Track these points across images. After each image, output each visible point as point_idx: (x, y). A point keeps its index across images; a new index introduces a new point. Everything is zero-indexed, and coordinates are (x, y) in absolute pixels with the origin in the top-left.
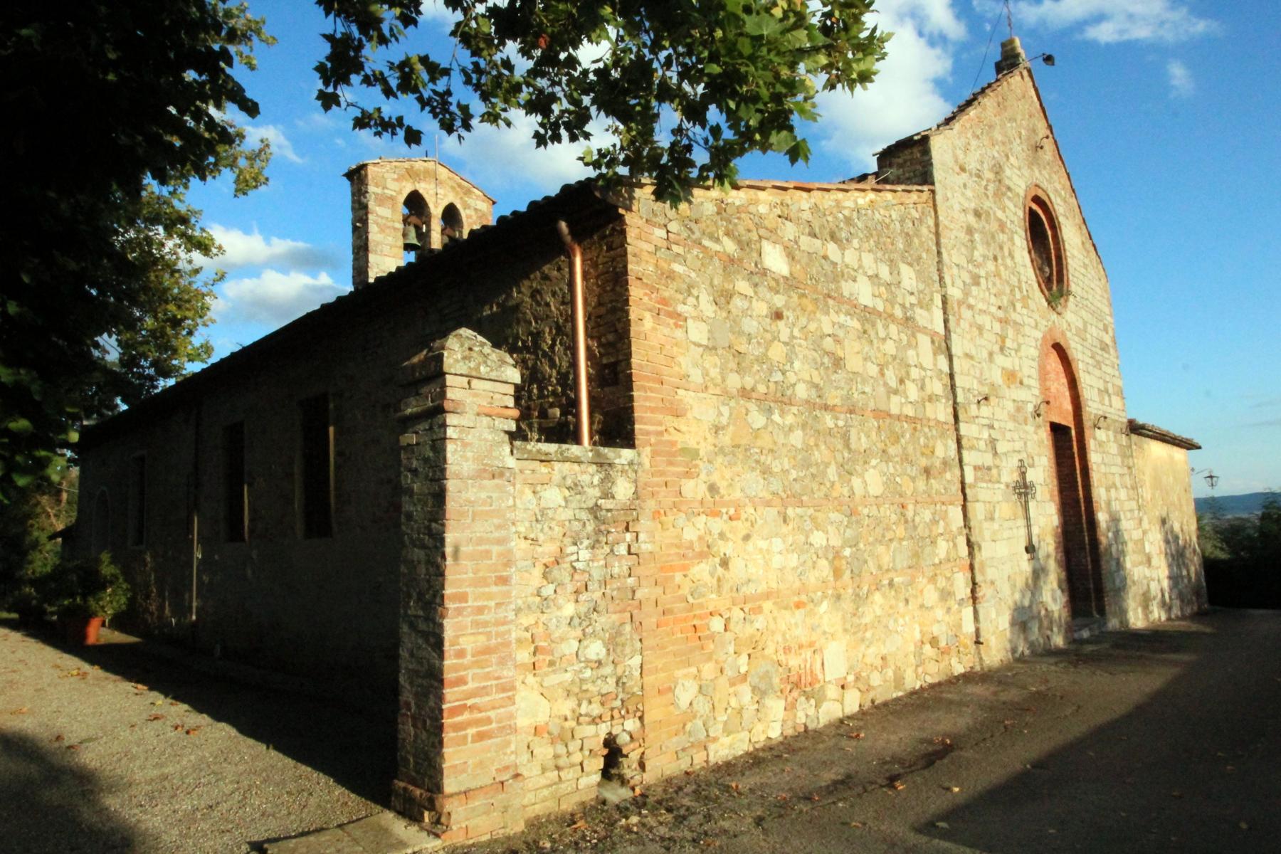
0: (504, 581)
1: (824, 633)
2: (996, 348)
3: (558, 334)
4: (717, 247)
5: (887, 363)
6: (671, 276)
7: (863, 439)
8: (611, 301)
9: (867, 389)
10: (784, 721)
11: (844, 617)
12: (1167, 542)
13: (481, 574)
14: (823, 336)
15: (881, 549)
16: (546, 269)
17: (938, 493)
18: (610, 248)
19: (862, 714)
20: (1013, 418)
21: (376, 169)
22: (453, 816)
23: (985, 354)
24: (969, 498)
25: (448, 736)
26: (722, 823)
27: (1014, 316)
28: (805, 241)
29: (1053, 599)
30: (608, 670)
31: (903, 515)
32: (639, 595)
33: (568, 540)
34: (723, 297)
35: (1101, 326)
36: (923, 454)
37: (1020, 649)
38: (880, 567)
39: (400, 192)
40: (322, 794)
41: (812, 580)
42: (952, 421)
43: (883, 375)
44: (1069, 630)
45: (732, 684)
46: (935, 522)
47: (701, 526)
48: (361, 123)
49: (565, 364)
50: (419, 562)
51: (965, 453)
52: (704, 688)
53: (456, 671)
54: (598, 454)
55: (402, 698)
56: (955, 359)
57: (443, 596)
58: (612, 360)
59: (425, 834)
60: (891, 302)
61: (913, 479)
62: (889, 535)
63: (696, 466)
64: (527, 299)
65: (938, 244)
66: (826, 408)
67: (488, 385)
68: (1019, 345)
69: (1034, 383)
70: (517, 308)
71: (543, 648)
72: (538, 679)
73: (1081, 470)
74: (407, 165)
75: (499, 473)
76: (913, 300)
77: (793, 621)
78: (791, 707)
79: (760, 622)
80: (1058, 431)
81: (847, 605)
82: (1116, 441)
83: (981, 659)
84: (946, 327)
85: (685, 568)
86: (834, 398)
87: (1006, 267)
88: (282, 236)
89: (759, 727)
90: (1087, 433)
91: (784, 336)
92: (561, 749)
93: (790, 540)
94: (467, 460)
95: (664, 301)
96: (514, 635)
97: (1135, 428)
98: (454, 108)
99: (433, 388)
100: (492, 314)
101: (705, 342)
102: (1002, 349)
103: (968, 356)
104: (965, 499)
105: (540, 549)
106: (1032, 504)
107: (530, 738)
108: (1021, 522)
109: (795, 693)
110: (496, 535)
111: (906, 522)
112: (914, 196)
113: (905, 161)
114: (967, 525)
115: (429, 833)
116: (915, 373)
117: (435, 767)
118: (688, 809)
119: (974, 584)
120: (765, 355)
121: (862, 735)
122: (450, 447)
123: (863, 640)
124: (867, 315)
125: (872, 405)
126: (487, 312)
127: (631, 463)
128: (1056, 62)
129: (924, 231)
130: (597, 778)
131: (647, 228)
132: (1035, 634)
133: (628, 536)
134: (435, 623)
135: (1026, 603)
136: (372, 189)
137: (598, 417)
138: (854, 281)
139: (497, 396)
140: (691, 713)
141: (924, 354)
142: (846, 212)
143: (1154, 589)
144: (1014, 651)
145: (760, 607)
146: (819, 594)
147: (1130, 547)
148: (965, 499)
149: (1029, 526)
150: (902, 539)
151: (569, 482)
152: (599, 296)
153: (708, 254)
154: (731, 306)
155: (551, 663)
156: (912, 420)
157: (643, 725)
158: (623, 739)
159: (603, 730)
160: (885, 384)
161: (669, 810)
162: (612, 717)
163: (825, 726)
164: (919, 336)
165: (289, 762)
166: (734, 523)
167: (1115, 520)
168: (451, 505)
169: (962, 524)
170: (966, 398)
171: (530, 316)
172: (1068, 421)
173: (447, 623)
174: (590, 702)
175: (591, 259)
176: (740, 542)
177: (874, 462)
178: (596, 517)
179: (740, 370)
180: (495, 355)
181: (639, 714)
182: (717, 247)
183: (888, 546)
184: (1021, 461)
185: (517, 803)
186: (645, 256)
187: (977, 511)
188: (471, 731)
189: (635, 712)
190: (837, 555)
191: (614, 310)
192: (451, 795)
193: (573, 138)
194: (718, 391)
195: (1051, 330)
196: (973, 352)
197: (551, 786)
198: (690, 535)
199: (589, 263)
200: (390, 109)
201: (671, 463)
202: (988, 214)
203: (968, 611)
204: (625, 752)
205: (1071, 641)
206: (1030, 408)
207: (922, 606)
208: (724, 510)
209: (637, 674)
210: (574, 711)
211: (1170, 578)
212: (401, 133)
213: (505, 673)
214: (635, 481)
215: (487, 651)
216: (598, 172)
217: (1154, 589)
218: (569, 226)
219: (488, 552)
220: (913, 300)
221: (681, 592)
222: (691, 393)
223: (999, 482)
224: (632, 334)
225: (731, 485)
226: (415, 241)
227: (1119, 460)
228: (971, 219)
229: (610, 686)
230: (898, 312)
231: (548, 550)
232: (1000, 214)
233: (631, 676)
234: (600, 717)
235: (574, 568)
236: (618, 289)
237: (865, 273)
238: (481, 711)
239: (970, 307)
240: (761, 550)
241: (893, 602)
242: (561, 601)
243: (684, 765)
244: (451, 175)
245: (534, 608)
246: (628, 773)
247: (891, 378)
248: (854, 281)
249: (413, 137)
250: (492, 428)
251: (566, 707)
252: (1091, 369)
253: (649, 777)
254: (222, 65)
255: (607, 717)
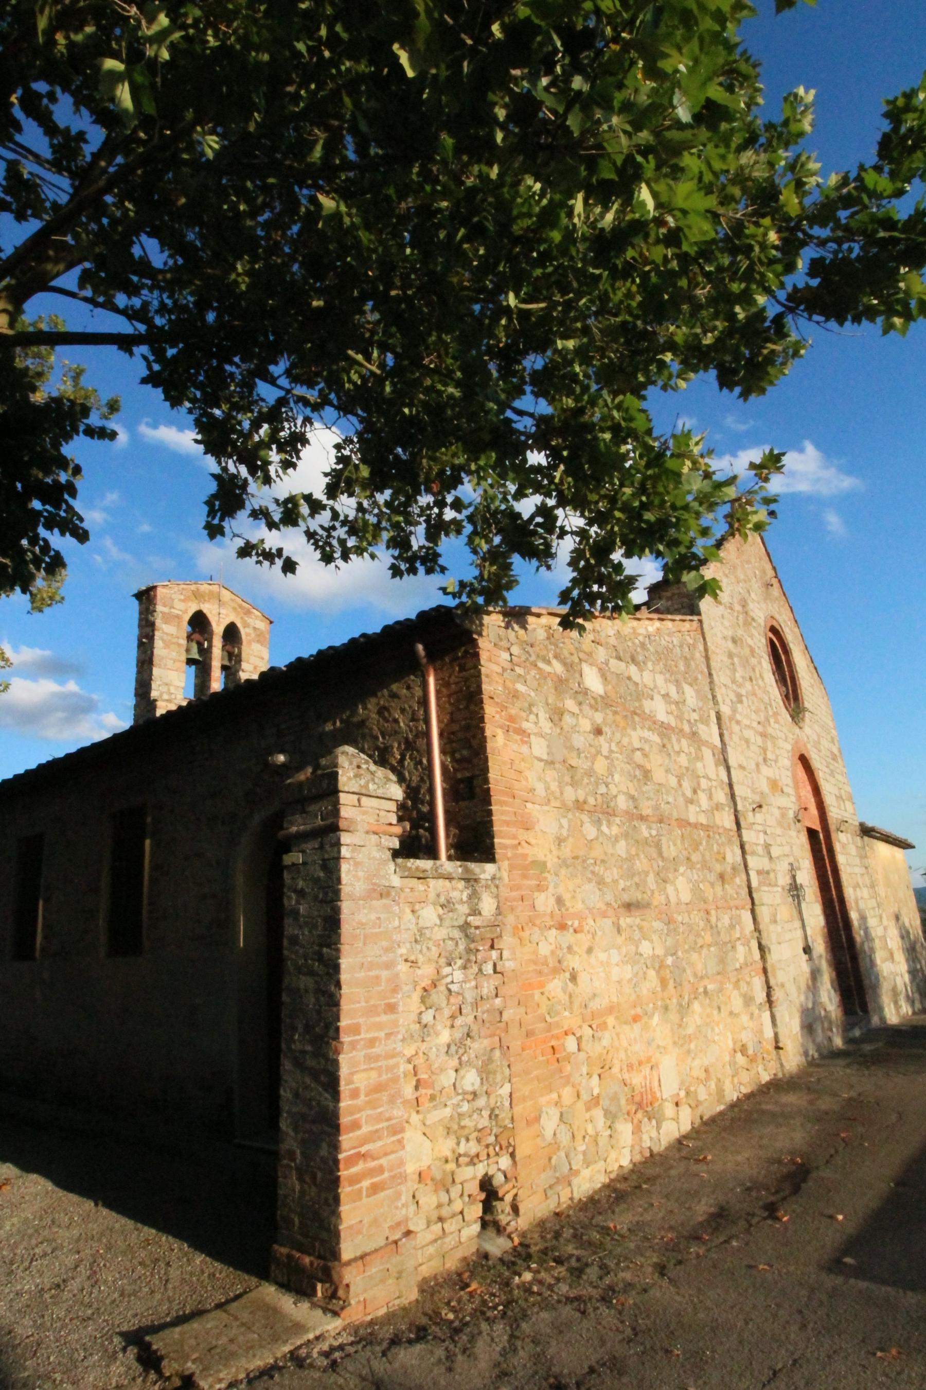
0: (391, 1008)
1: (658, 1047)
2: (761, 759)
3: (407, 749)
4: (547, 669)
5: (683, 774)
6: (516, 695)
7: (672, 847)
8: (465, 719)
9: (671, 800)
10: (632, 1146)
11: (672, 1030)
12: (902, 937)
13: (372, 1002)
14: (634, 750)
15: (694, 956)
16: (394, 687)
17: (732, 898)
18: (462, 668)
19: (695, 1133)
20: (780, 824)
21: (164, 590)
22: (352, 1288)
23: (753, 766)
24: (756, 902)
25: (345, 1191)
26: (621, 1275)
27: (770, 731)
28: (613, 662)
29: (829, 999)
30: (481, 1102)
31: (708, 921)
32: (506, 1016)
33: (442, 961)
34: (557, 715)
35: (829, 738)
36: (717, 860)
37: (811, 1053)
38: (695, 975)
39: (185, 612)
40: (179, 1269)
41: (645, 992)
42: (735, 828)
43: (680, 786)
44: (847, 1027)
45: (588, 1109)
46: (732, 927)
47: (552, 940)
48: (244, 552)
49: (415, 779)
50: (307, 991)
51: (749, 858)
52: (565, 1115)
53: (352, 1114)
54: (467, 870)
55: (284, 1147)
56: (733, 772)
57: (338, 1029)
58: (468, 774)
59: (319, 1312)
60: (680, 718)
61: (712, 885)
62: (700, 942)
63: (545, 879)
64: (374, 716)
65: (709, 667)
66: (642, 818)
67: (374, 802)
68: (777, 756)
69: (790, 790)
70: (362, 723)
71: (425, 1082)
72: (420, 1116)
73: (832, 871)
74: (193, 587)
75: (385, 893)
76: (695, 716)
77: (632, 1036)
78: (637, 1130)
79: (606, 1039)
80: (812, 833)
81: (674, 1016)
82: (854, 843)
83: (782, 1065)
84: (722, 740)
85: (542, 985)
86: (646, 809)
87: (759, 687)
88: (30, 645)
89: (613, 1155)
90: (834, 835)
91: (605, 752)
92: (444, 1198)
93: (624, 950)
94: (359, 880)
95: (511, 719)
96: (402, 1069)
97: (867, 831)
98: (335, 542)
99: (325, 806)
100: (335, 729)
101: (545, 757)
102: (765, 760)
103: (741, 767)
104: (753, 903)
105: (419, 972)
106: (803, 905)
107: (416, 1186)
108: (797, 924)
109: (640, 1115)
110: (384, 958)
111: (712, 927)
112: (687, 625)
113: (673, 595)
114: (757, 929)
115: (325, 1310)
116: (704, 783)
117: (328, 1230)
118: (578, 1259)
119: (769, 987)
120: (592, 769)
121: (709, 1157)
122: (344, 867)
123: (689, 1052)
124: (664, 730)
125: (675, 815)
126: (329, 727)
127: (493, 878)
128: (779, 516)
129: (698, 655)
130: (476, 1227)
131: (496, 651)
132: (820, 1038)
133: (494, 954)
134: (327, 1059)
135: (810, 1006)
136: (159, 608)
137: (454, 831)
138: (652, 699)
139: (382, 813)
140: (555, 1145)
141: (709, 766)
142: (641, 638)
143: (900, 987)
144: (806, 1053)
145: (605, 1023)
146: (651, 1005)
147: (877, 944)
148: (753, 903)
149: (804, 927)
150: (709, 946)
151: (442, 900)
152: (452, 714)
153: (544, 676)
154: (563, 723)
155: (432, 1098)
156: (706, 828)
157: (515, 1162)
158: (499, 1179)
159: (480, 1170)
160: (684, 795)
161: (559, 1261)
162: (488, 1155)
163: (667, 1149)
164: (704, 749)
165: (130, 1224)
166: (579, 936)
167: (863, 918)
168: (346, 929)
169: (752, 927)
170: (744, 806)
171: (376, 731)
172: (817, 826)
173: (343, 1059)
174: (468, 1140)
175: (443, 679)
176: (585, 956)
177: (682, 869)
178: (467, 936)
179: (574, 784)
180: (381, 773)
181: (511, 1150)
182: (547, 669)
183: (700, 954)
184: (791, 864)
185: (410, 1264)
186: (496, 678)
187: (764, 913)
188: (366, 1183)
189: (507, 1147)
190: (662, 966)
191: (467, 728)
192: (349, 1263)
193: (429, 571)
194: (558, 804)
195: (797, 742)
196: (745, 764)
197: (435, 1241)
198: (544, 950)
199: (442, 684)
200: (272, 539)
201: (525, 877)
202: (741, 640)
203: (767, 1015)
204: (500, 1195)
205: (849, 1041)
206: (791, 814)
207: (731, 1013)
208: (570, 923)
209: (507, 1104)
210: (454, 1152)
211: (909, 972)
212: (279, 563)
213: (395, 1113)
214: (497, 896)
215: (378, 1088)
216: (457, 601)
217: (900, 987)
218: (425, 649)
219: (377, 977)
220: (695, 716)
221: (540, 1011)
222: (537, 807)
223: (776, 885)
224: (489, 750)
225: (574, 897)
226: (197, 657)
227: (857, 860)
228: (730, 645)
229: (484, 1122)
230: (686, 728)
231: (426, 972)
232: (749, 641)
233: (501, 1108)
234: (477, 1156)
235: (449, 990)
236: (472, 707)
237: (659, 692)
238: (374, 1159)
239: (738, 722)
240: (602, 962)
241: (709, 1010)
242: (439, 1027)
243: (551, 1205)
244: (233, 597)
245: (416, 1037)
246: (503, 1219)
247: (687, 786)
248: (652, 699)
249: (290, 567)
250: (379, 845)
251: (446, 1147)
252: (828, 777)
253: (522, 1223)
254: (66, 497)
255: (483, 1156)
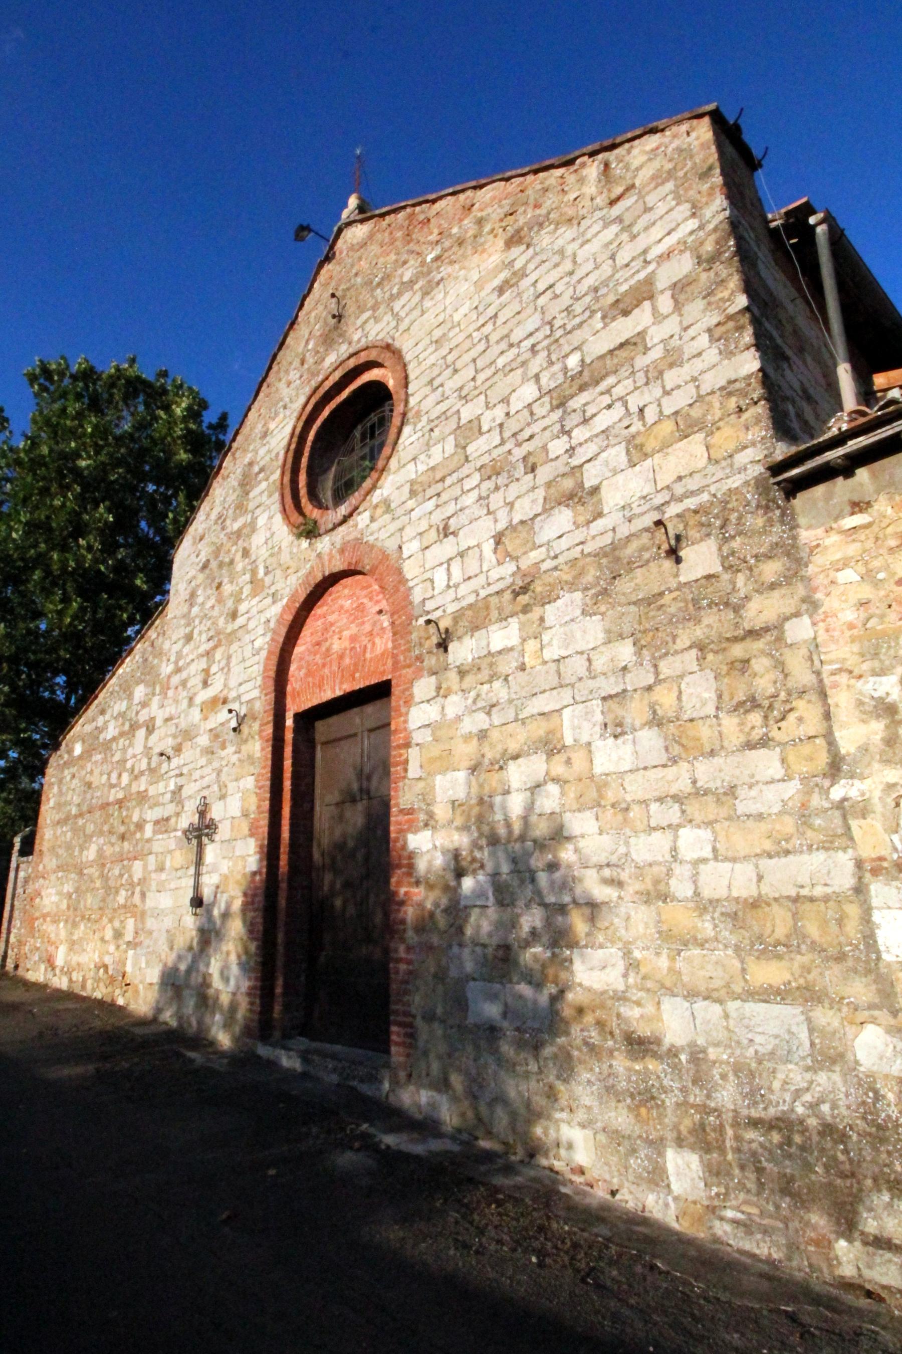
46: (121, 875)
135: (183, 967)
223: (175, 830)
